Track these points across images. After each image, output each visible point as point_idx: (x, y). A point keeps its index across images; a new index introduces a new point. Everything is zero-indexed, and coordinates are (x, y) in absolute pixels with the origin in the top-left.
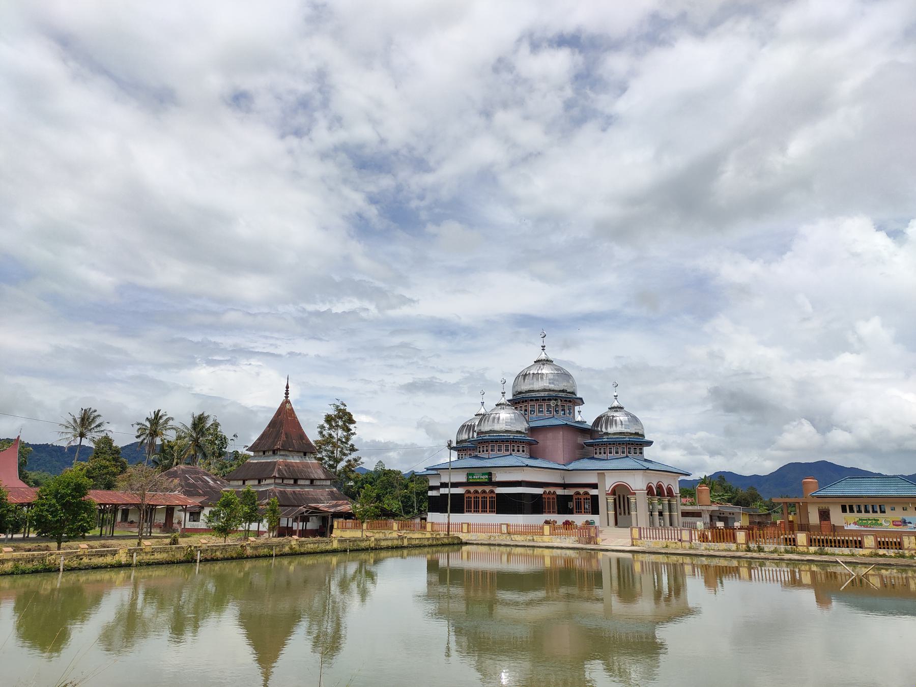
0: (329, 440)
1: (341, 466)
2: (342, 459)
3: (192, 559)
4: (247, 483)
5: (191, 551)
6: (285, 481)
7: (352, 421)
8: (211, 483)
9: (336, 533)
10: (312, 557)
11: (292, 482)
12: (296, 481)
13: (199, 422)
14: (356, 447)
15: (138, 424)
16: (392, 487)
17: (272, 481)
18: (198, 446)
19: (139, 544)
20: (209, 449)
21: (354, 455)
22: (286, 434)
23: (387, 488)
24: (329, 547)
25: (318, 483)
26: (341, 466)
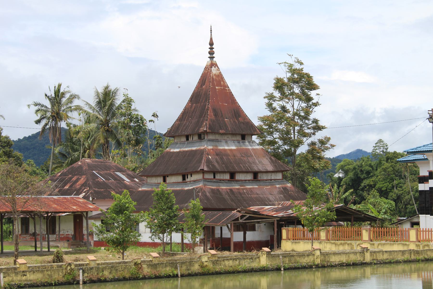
0: (281, 115)
1: (303, 149)
2: (300, 143)
3: (74, 279)
4: (169, 180)
5: (72, 270)
6: (218, 176)
7: (312, 86)
8: (127, 180)
9: (287, 246)
10: (231, 277)
11: (227, 177)
12: (232, 175)
13: (106, 99)
14: (321, 123)
15: (36, 105)
16: (401, 177)
17: (199, 177)
18: (110, 132)
19: (15, 262)
20: (123, 135)
21: (320, 135)
22: (214, 110)
23: (392, 180)
24: (255, 265)
25: (264, 177)
26: (303, 149)
